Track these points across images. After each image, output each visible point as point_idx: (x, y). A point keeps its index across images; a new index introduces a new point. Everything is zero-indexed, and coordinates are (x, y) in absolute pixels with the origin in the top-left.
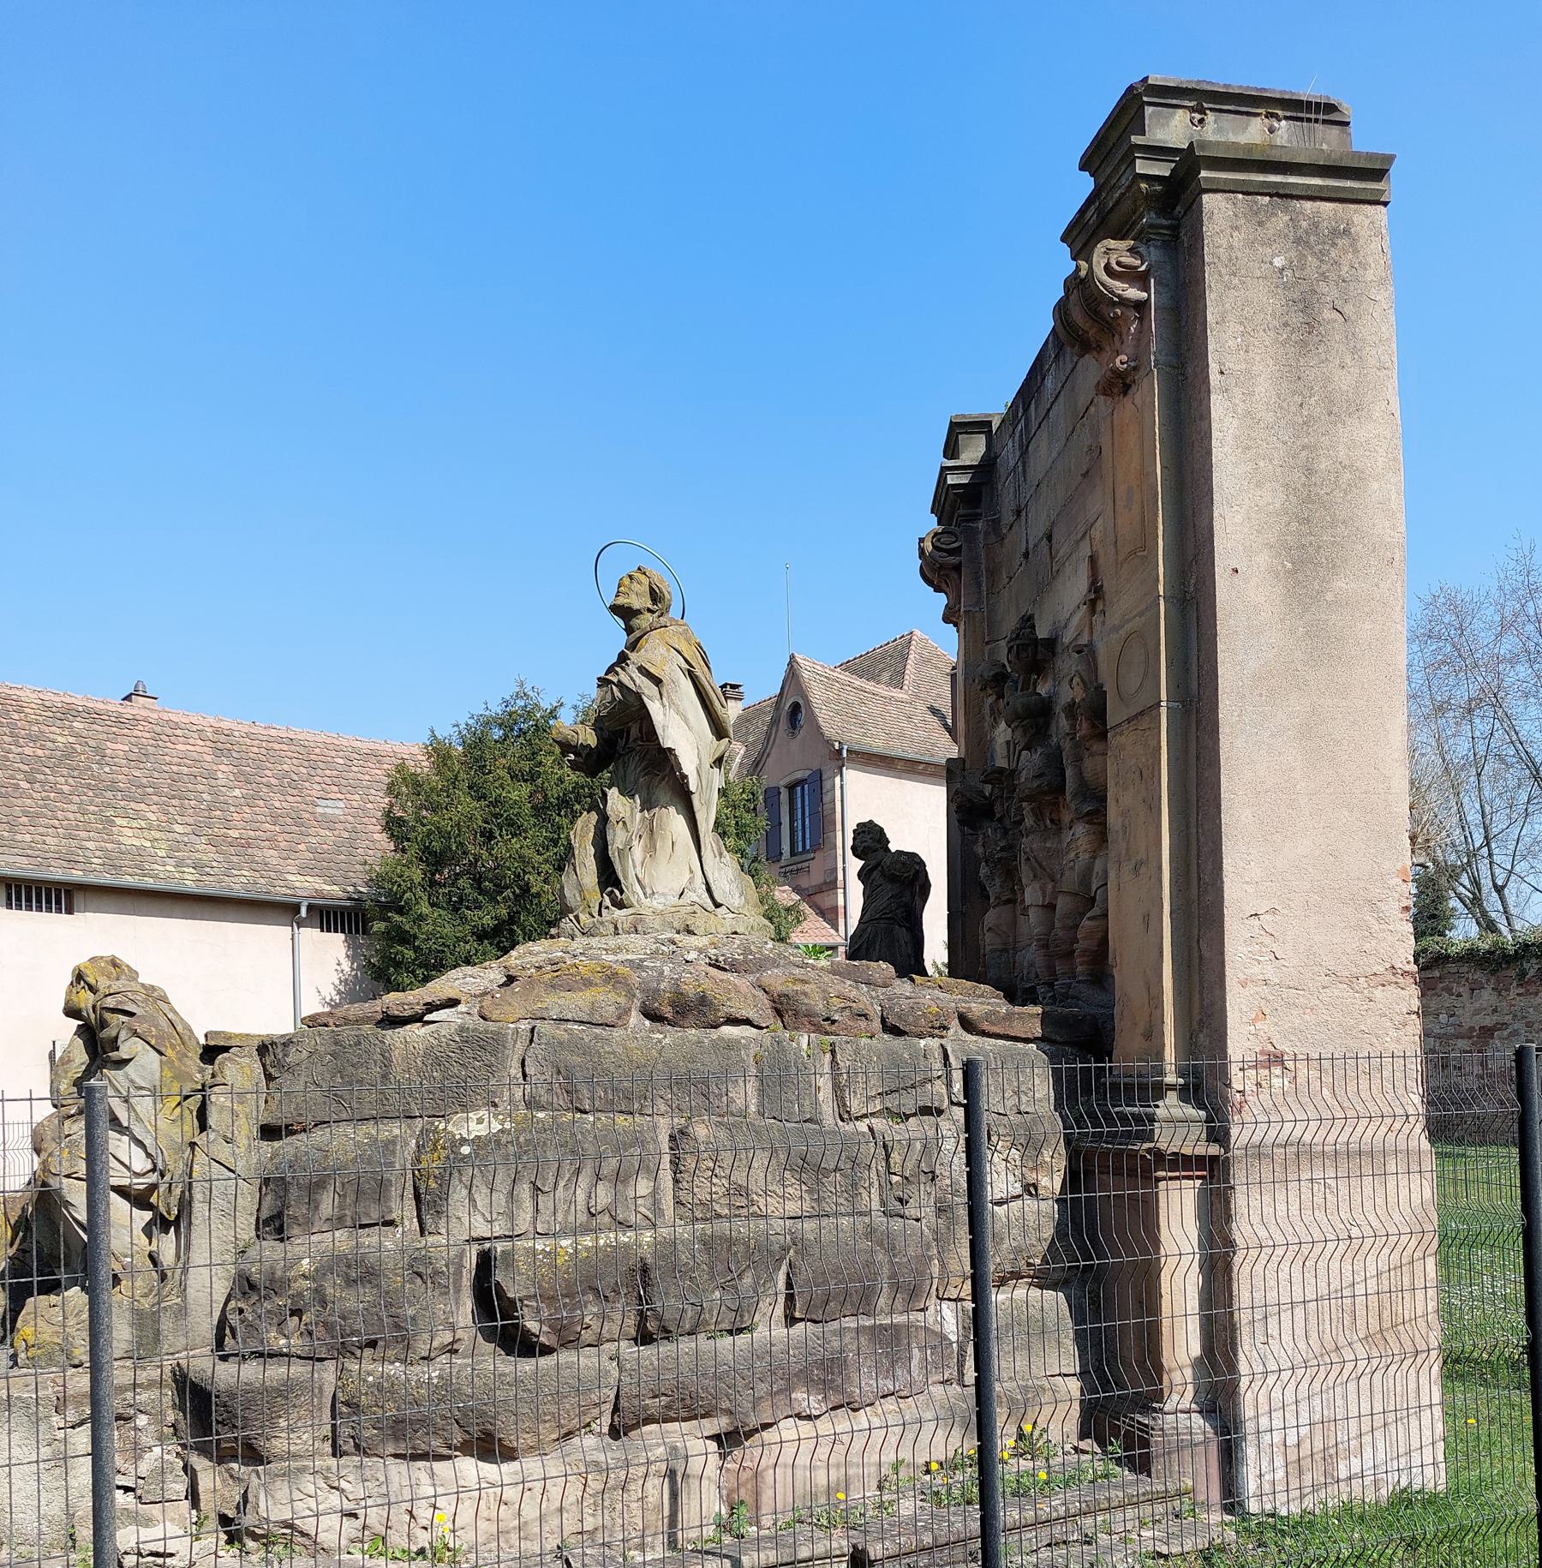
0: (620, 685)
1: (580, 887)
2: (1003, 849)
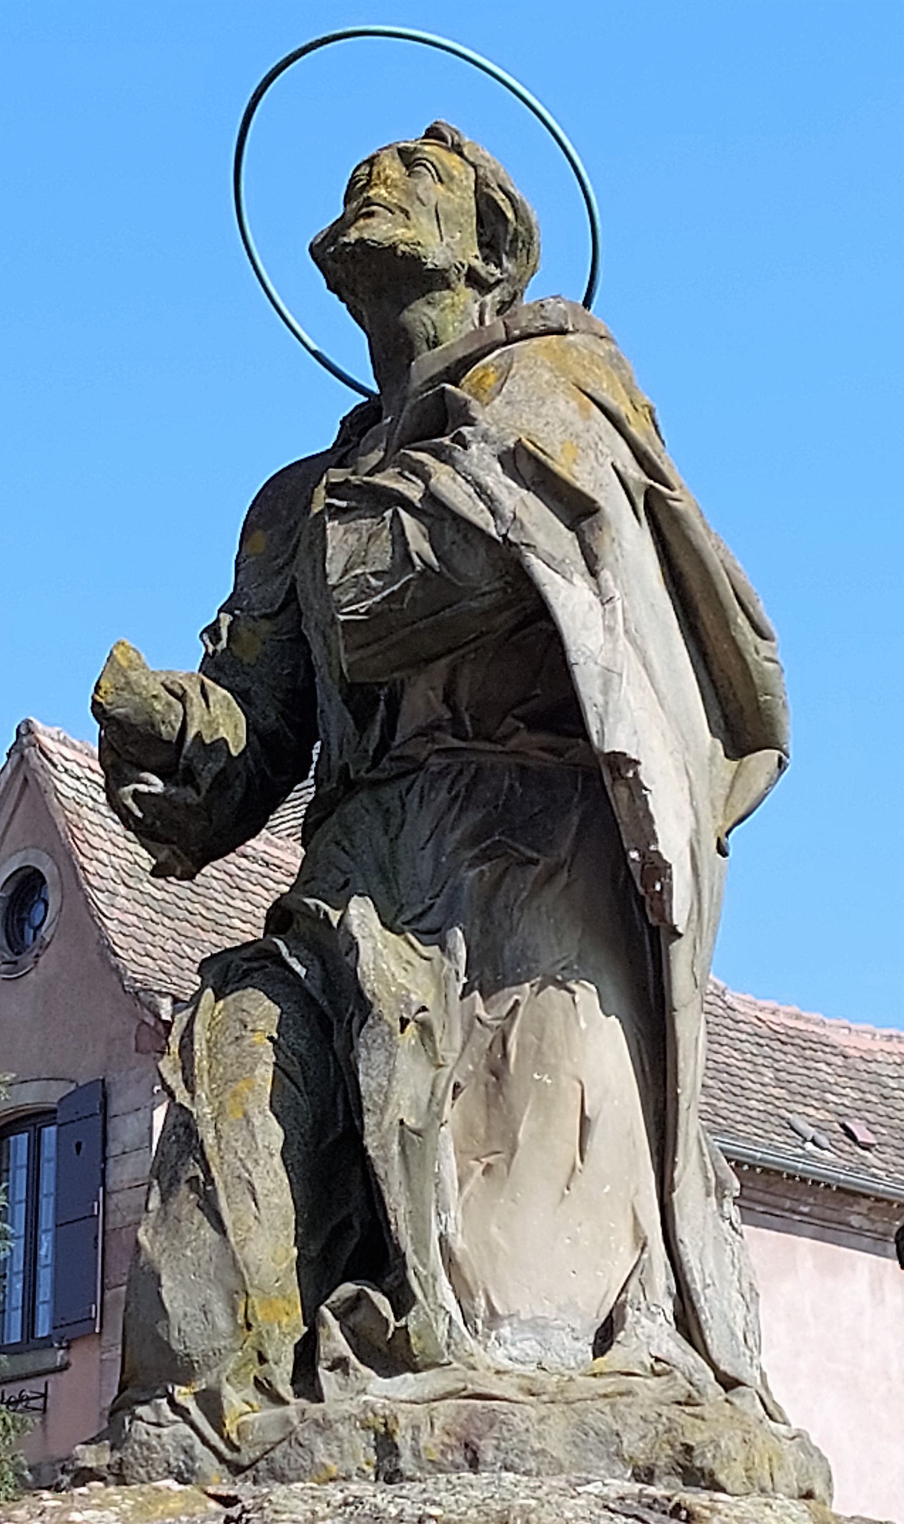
0: (435, 511)
1: (236, 1284)
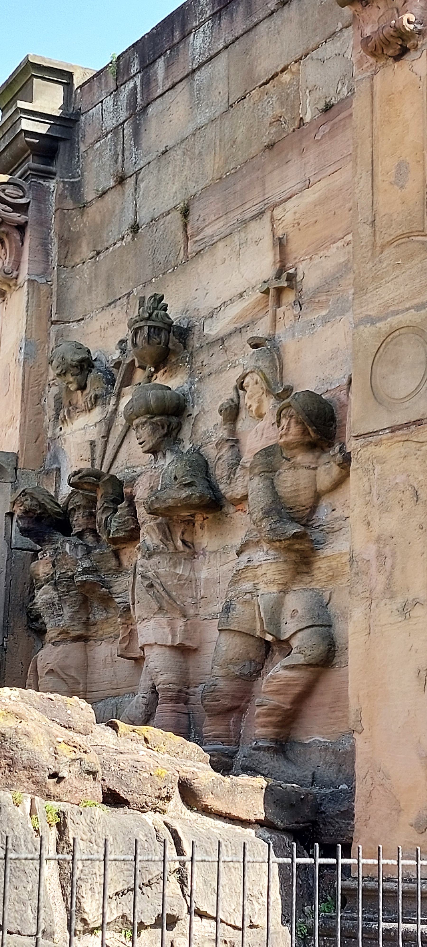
2: (86, 571)
